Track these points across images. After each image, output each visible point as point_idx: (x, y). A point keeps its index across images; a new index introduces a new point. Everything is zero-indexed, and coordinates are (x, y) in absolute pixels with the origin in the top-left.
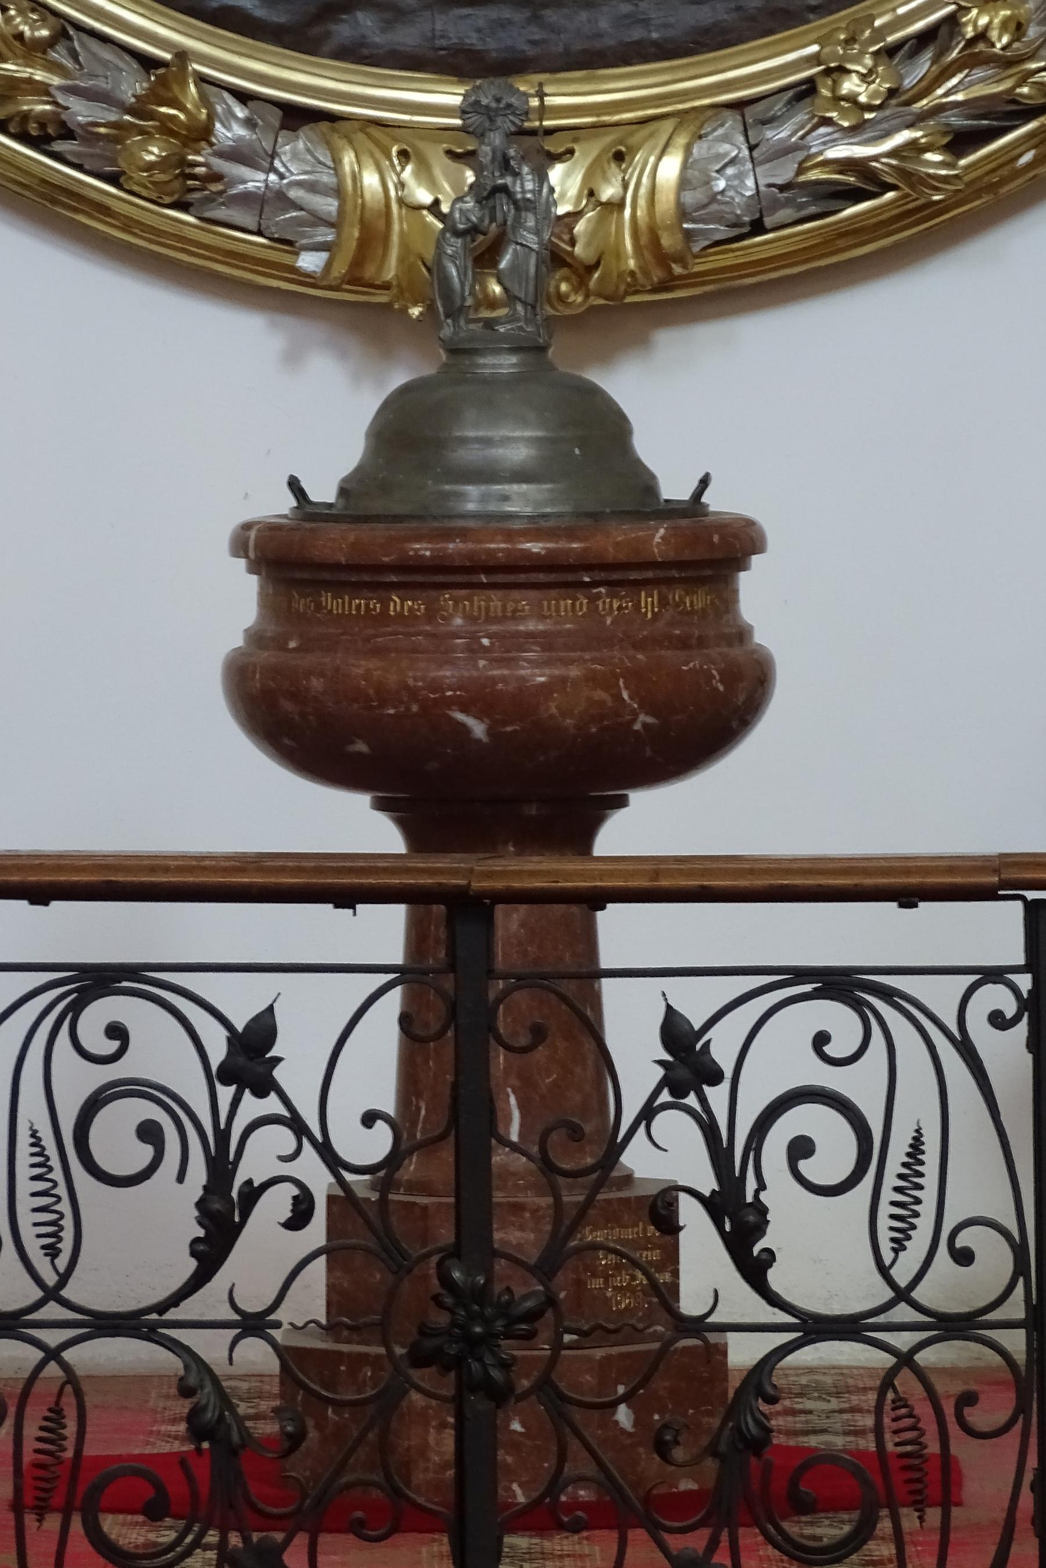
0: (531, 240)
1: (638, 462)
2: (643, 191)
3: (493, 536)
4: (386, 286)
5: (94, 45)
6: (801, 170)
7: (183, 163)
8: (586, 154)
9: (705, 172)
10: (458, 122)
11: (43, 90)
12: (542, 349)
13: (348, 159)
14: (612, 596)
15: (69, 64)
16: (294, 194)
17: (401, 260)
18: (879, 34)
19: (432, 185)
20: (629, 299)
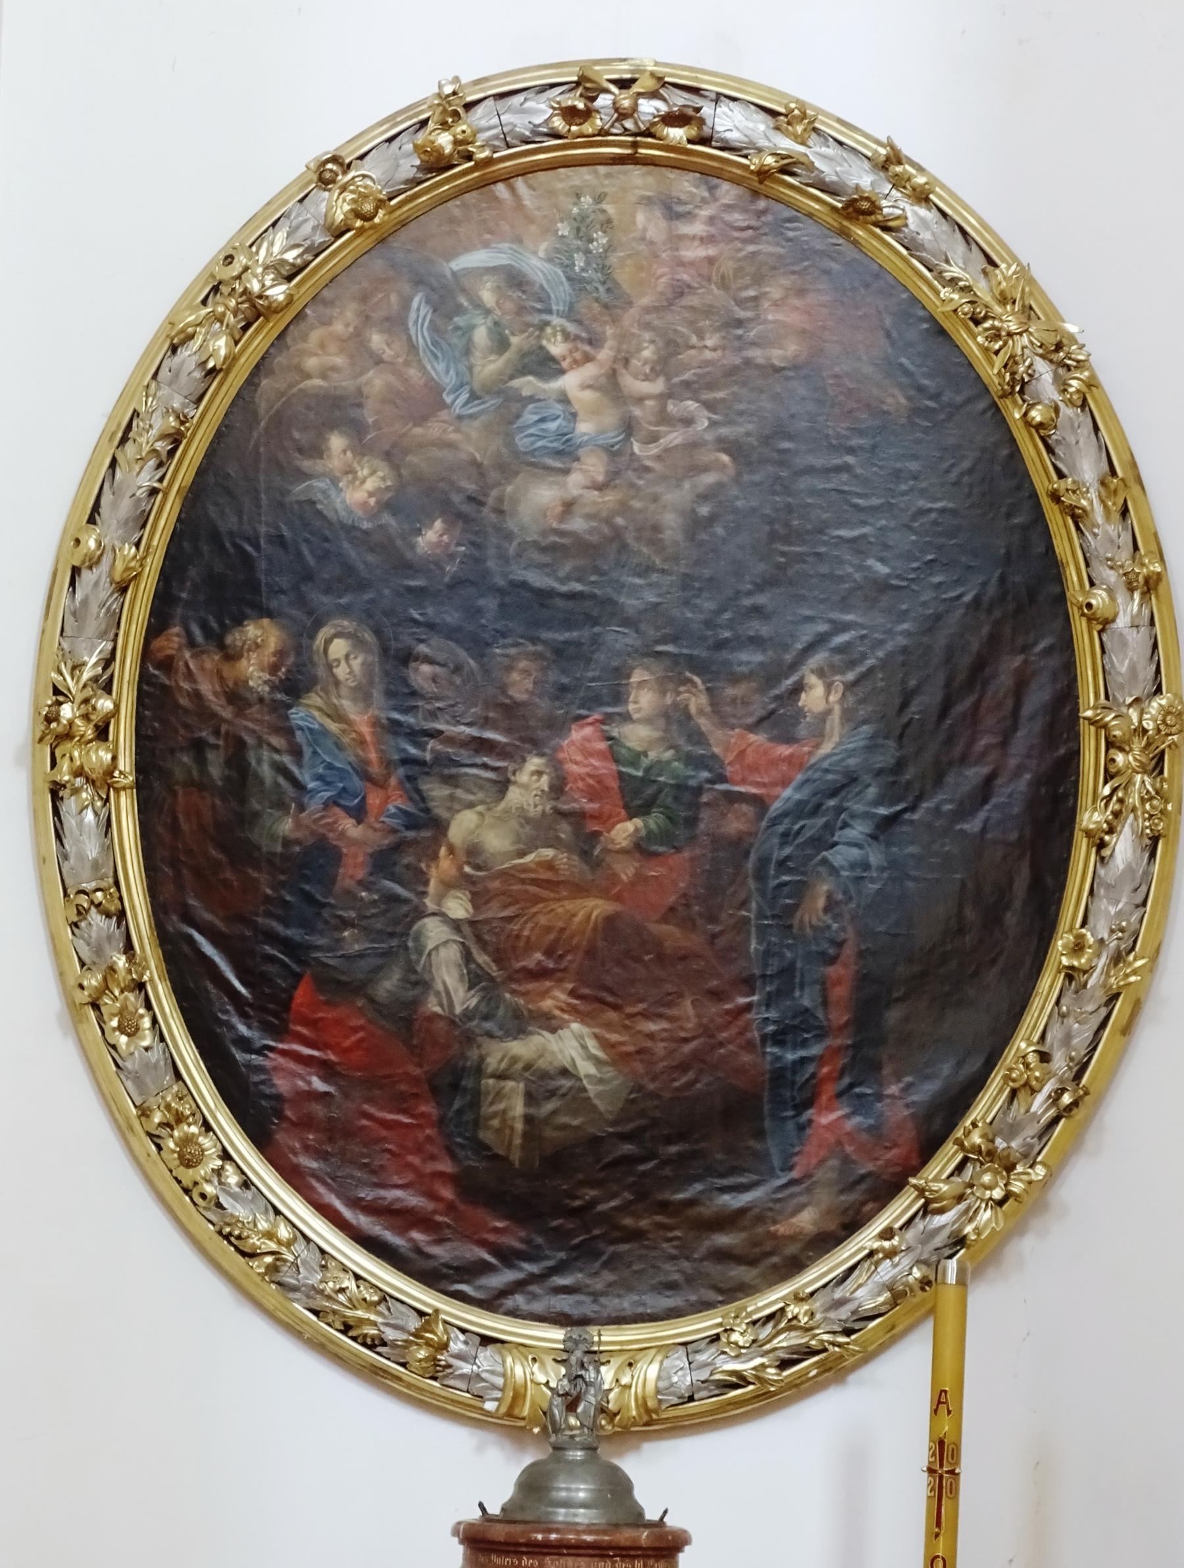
0: (592, 1400)
1: (636, 1503)
2: (641, 1380)
3: (570, 1532)
4: (523, 1419)
5: (398, 1305)
6: (711, 1374)
7: (435, 1359)
8: (616, 1362)
9: (668, 1373)
10: (562, 1346)
11: (374, 1324)
12: (595, 1449)
13: (509, 1360)
14: (622, 1561)
15: (386, 1313)
16: (484, 1375)
17: (532, 1406)
18: (749, 1314)
19: (546, 1373)
20: (633, 1429)
